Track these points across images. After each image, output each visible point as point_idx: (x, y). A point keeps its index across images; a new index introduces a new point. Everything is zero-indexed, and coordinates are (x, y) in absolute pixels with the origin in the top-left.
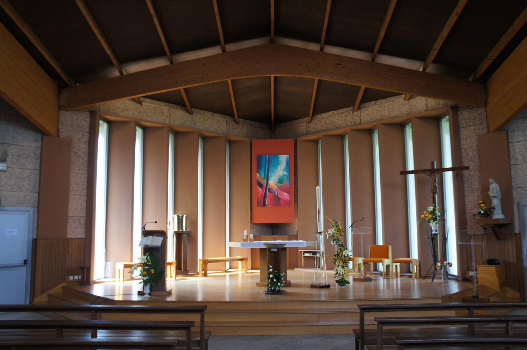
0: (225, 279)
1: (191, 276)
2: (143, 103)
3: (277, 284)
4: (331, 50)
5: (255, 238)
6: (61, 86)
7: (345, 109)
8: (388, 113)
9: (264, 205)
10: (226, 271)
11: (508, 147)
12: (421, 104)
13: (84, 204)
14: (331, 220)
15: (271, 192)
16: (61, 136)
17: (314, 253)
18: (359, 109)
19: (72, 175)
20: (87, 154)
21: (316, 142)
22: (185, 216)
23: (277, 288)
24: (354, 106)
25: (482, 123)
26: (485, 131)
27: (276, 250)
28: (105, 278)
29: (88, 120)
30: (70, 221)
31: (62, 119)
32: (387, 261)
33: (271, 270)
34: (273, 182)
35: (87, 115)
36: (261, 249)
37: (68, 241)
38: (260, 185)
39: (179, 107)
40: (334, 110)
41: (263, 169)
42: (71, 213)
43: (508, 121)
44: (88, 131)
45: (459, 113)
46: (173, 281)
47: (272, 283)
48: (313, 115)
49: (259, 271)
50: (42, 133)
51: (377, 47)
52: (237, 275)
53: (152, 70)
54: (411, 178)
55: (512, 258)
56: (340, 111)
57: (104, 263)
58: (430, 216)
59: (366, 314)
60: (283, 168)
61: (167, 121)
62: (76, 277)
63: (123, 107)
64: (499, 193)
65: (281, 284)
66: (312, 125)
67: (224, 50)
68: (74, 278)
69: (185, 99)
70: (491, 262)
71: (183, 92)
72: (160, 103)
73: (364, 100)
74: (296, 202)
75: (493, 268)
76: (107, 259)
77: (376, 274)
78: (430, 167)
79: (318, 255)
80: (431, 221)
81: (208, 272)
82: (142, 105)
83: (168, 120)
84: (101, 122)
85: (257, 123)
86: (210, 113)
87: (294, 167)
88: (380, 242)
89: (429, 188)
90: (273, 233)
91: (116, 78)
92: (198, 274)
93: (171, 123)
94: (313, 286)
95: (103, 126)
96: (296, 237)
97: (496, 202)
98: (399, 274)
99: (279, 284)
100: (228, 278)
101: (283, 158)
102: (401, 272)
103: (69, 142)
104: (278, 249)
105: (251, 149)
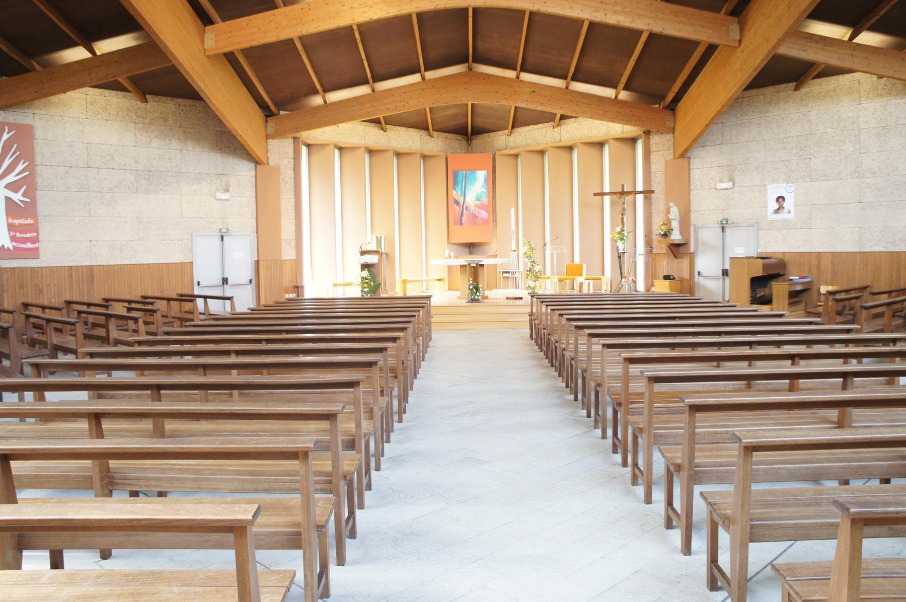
4: (526, 77)
5: (456, 257)
6: (268, 113)
9: (461, 224)
11: (689, 174)
13: (294, 228)
16: (271, 164)
18: (559, 125)
25: (669, 149)
26: (672, 157)
30: (283, 244)
31: (270, 147)
32: (580, 279)
35: (291, 141)
37: (282, 262)
38: (457, 203)
41: (460, 186)
42: (283, 236)
43: (687, 150)
45: (25, 553)
48: (513, 127)
50: (257, 162)
51: (570, 75)
53: (355, 98)
54: (607, 199)
55: (686, 275)
56: (540, 126)
59: (757, 456)
64: (678, 216)
66: (511, 139)
67: (423, 79)
70: (667, 278)
74: (495, 220)
75: (667, 282)
78: (620, 190)
79: (517, 275)
85: (452, 135)
86: (404, 128)
89: (620, 209)
91: (318, 108)
94: (507, 298)
96: (495, 256)
97: (675, 225)
101: (481, 175)
103: (277, 169)
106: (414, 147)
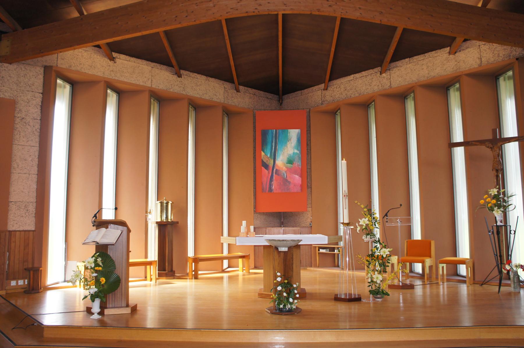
0: (222, 281)
1: (179, 278)
2: (117, 60)
3: (288, 299)
7: (371, 71)
8: (427, 72)
10: (223, 271)
12: (477, 55)
13: (34, 186)
14: (362, 206)
15: (278, 175)
17: (333, 249)
19: (15, 147)
20: (39, 122)
21: (333, 113)
22: (170, 202)
23: (289, 306)
24: (381, 66)
27: (285, 249)
28: (65, 281)
29: (41, 77)
33: (279, 279)
34: (281, 161)
36: (265, 246)
38: (266, 166)
39: (165, 67)
40: (356, 73)
41: (269, 147)
44: (41, 91)
46: (145, 289)
47: (280, 299)
49: (262, 271)
52: (238, 276)
54: (459, 153)
56: (364, 73)
57: (64, 262)
58: (494, 201)
60: (293, 145)
61: (148, 84)
62: (21, 282)
63: (85, 60)
65: (294, 299)
66: (328, 93)
68: (17, 283)
69: (171, 55)
71: (162, 35)
72: (139, 61)
73: (397, 57)
76: (67, 258)
77: (412, 277)
78: (490, 137)
79: (336, 251)
80: (496, 208)
81: (199, 272)
82: (115, 62)
83: (150, 82)
84: (59, 81)
86: (204, 77)
87: (306, 144)
88: (417, 235)
90: (282, 224)
92: (187, 274)
93: (154, 86)
95: (65, 87)
98: (445, 277)
99: (291, 300)
100: (225, 280)
101: (294, 134)
102: (447, 275)
104: (290, 248)
105: (254, 123)
106: (215, 99)
